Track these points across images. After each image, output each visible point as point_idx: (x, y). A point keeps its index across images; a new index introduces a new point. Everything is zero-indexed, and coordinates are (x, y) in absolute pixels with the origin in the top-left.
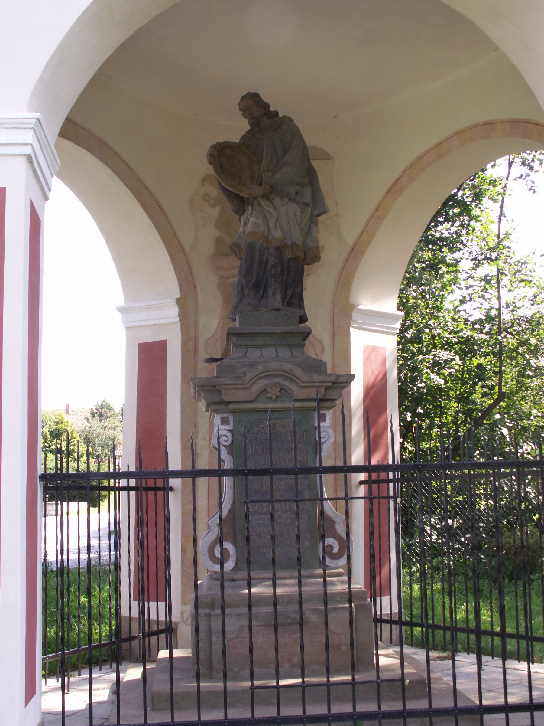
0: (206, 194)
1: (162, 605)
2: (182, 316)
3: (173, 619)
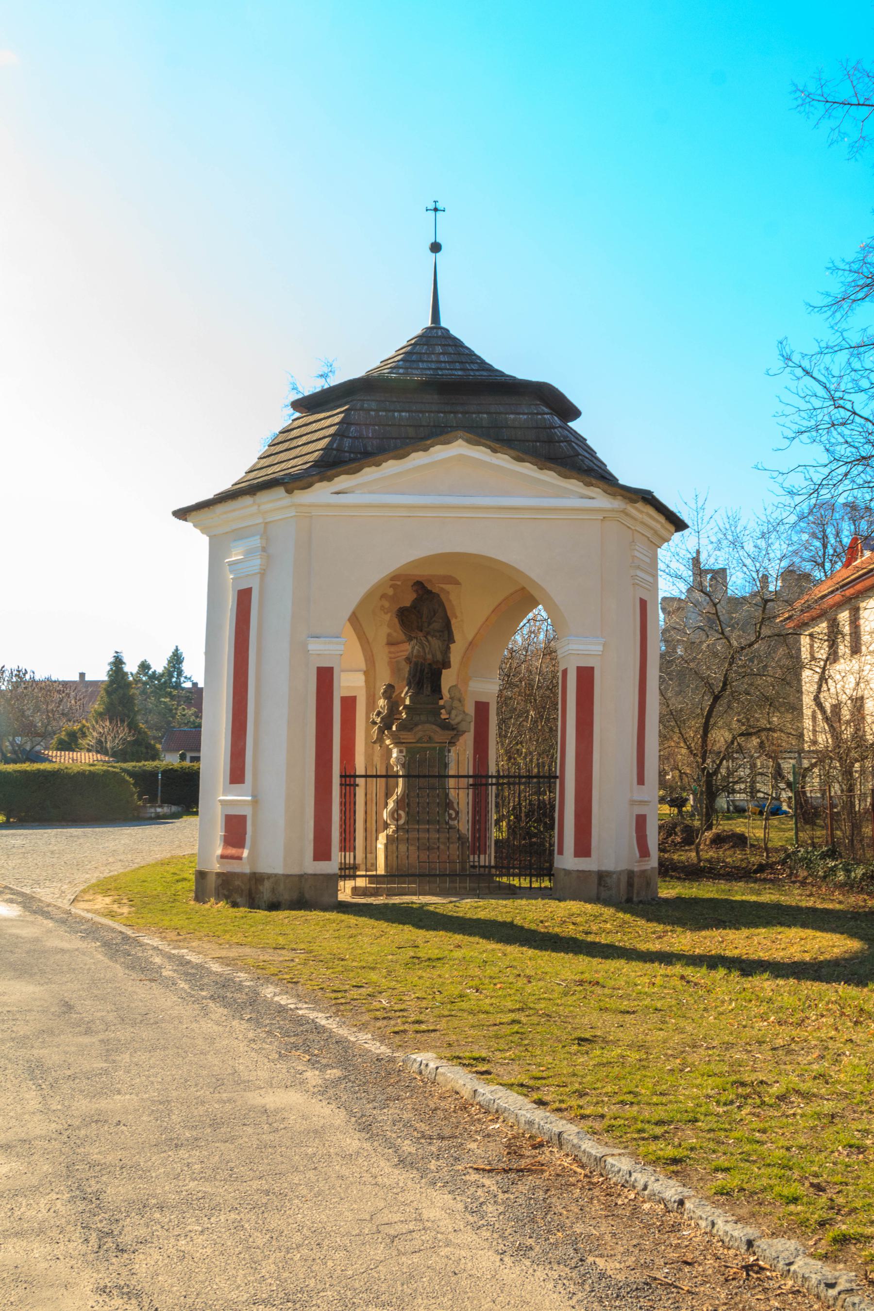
0: (382, 606)
1: (352, 854)
2: (367, 681)
3: (357, 862)
